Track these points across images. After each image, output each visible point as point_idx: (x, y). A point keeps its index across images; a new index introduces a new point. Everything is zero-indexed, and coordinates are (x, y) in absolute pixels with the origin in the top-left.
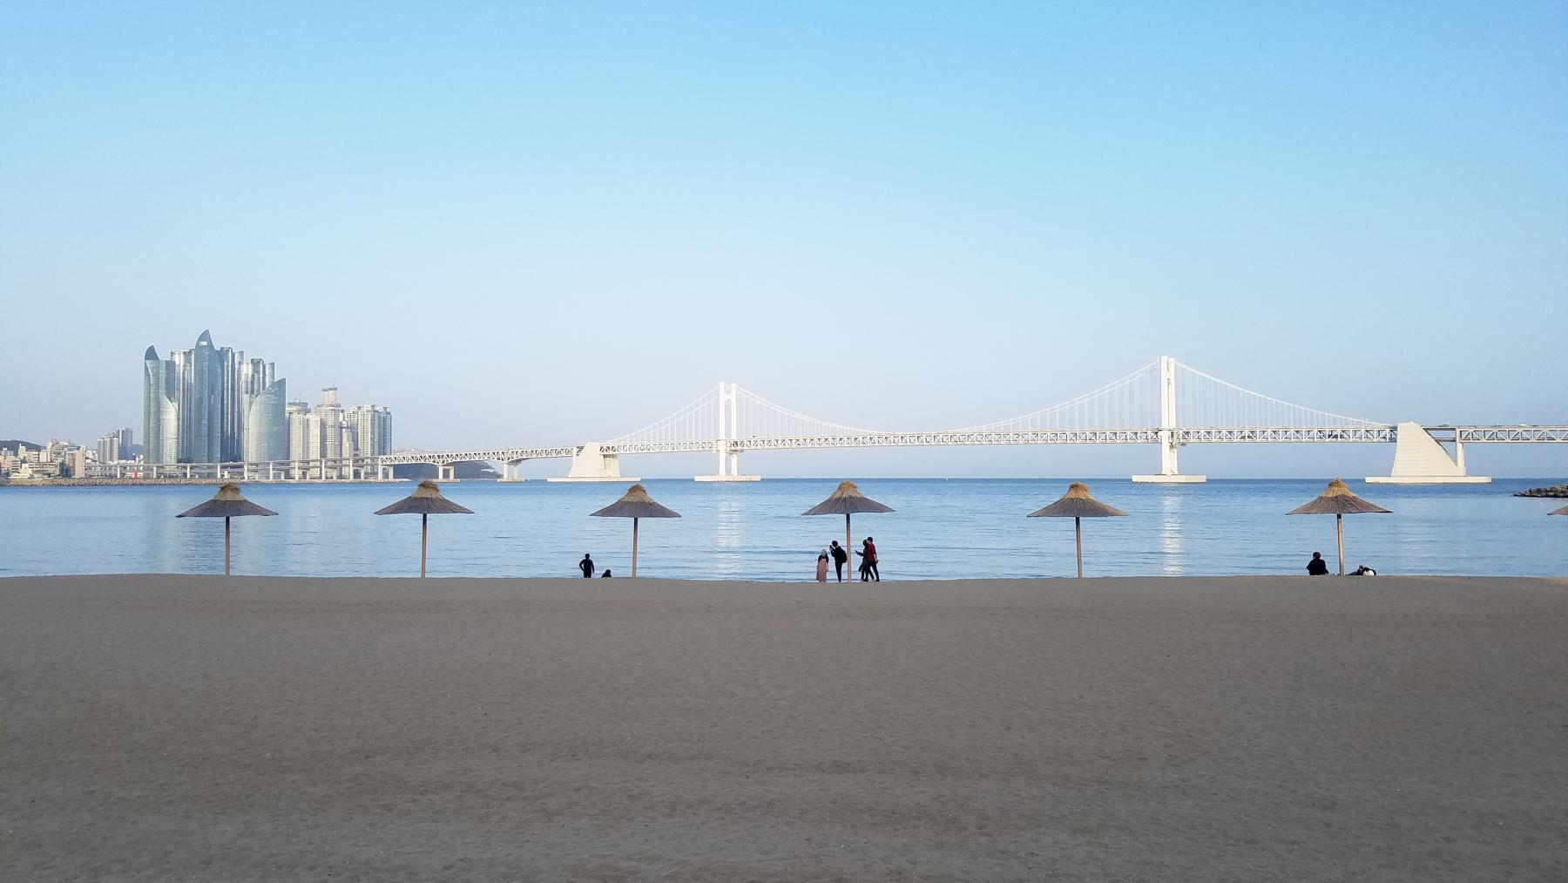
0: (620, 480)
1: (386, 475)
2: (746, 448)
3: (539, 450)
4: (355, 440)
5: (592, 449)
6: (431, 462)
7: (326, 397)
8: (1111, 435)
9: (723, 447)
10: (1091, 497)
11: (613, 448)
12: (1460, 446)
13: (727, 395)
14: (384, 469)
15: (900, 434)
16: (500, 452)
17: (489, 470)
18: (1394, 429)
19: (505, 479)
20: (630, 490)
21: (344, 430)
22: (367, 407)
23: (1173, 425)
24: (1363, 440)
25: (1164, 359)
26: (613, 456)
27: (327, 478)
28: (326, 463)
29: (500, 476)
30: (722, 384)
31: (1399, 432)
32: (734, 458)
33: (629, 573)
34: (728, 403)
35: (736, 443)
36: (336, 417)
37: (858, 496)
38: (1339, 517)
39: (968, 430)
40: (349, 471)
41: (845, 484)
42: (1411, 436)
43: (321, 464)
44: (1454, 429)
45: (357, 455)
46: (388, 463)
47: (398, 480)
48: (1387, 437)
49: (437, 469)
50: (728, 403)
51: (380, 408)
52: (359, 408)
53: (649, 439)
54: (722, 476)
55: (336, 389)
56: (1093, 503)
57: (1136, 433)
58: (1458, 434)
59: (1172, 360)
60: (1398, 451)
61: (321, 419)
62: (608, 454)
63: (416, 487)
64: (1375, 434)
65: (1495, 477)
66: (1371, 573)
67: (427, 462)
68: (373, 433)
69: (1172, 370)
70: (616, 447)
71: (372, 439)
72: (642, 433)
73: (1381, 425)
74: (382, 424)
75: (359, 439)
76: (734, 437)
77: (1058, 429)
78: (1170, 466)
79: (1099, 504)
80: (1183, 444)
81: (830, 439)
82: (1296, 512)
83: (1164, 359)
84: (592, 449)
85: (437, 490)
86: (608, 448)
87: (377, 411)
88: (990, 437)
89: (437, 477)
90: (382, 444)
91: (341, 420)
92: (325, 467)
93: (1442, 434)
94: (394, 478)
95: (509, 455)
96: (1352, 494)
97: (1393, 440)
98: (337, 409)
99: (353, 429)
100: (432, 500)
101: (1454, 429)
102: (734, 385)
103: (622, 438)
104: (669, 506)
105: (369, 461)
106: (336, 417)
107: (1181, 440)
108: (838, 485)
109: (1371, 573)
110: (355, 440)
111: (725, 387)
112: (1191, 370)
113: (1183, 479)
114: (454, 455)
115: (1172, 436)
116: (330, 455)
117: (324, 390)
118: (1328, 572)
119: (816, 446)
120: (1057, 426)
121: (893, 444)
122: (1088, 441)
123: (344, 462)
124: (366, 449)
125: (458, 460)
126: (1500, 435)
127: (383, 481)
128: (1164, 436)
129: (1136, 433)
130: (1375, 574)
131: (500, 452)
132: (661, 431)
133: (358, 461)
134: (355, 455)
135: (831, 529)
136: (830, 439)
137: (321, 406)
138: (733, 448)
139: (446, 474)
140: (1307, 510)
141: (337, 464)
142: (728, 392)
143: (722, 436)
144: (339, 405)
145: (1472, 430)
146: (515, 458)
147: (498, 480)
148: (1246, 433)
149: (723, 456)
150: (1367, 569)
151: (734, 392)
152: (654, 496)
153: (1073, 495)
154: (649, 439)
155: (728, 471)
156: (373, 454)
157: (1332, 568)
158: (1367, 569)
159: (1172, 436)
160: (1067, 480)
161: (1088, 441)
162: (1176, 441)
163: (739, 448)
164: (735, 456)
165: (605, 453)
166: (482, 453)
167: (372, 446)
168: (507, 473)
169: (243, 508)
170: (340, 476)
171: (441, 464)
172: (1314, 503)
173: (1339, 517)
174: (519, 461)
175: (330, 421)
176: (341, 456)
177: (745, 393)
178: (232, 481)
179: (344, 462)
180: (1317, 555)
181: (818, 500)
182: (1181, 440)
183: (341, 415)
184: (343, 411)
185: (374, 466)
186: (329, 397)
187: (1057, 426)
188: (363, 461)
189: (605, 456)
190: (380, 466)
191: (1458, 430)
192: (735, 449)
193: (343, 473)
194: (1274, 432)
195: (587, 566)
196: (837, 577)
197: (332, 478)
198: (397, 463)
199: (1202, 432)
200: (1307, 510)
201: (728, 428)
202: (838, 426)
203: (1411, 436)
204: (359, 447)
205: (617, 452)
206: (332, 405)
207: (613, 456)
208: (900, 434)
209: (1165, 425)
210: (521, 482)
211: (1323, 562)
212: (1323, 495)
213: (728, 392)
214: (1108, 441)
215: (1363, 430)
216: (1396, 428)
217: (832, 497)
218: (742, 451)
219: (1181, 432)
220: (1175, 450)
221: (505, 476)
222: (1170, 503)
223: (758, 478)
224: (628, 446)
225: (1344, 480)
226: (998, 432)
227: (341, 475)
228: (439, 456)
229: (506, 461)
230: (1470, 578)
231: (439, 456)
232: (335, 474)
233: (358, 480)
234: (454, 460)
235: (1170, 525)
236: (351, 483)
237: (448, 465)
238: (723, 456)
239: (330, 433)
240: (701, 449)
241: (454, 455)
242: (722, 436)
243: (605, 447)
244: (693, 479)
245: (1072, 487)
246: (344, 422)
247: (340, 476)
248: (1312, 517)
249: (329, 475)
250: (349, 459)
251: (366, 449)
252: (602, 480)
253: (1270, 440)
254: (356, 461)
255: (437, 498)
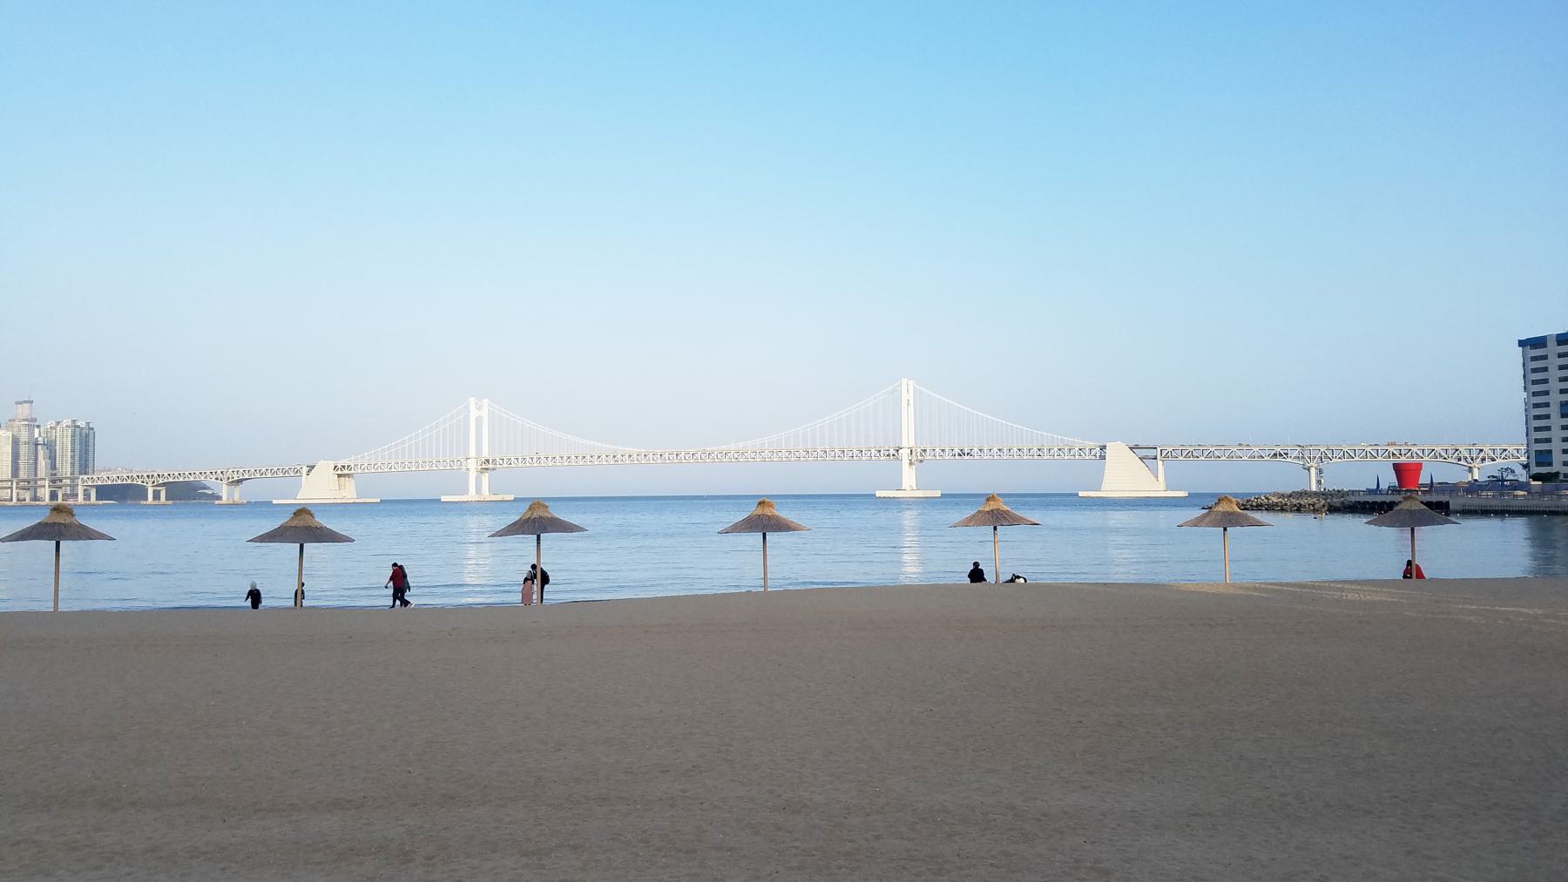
0: (357, 501)
1: (87, 496)
2: (498, 466)
3: (264, 470)
4: (52, 458)
5: (325, 468)
6: (139, 483)
7: (20, 410)
8: (822, 453)
9: (473, 465)
10: (777, 513)
11: (348, 466)
12: (1160, 463)
13: (479, 411)
14: (85, 490)
15: (659, 451)
16: (219, 472)
17: (206, 491)
18: (1103, 448)
19: (225, 500)
20: (295, 514)
21: (39, 447)
22: (67, 422)
23: (912, 444)
24: (1077, 457)
25: (904, 381)
26: (348, 475)
27: (18, 500)
28: (17, 483)
29: (220, 498)
30: (472, 400)
31: (1108, 450)
32: (485, 477)
33: (49, 607)
34: (479, 420)
35: (488, 461)
36: (31, 433)
37: (549, 516)
38: (995, 529)
39: (724, 448)
40: (45, 493)
41: (537, 504)
42: (1118, 452)
43: (12, 484)
44: (1156, 448)
45: (55, 475)
46: (90, 484)
47: (101, 502)
48: (1098, 455)
49: (145, 490)
50: (479, 420)
51: (82, 424)
52: (58, 423)
53: (383, 458)
54: (472, 495)
55: (31, 402)
56: (777, 518)
57: (880, 451)
58: (1159, 451)
59: (912, 382)
60: (1107, 467)
61: (13, 435)
62: (343, 473)
63: (49, 511)
64: (1087, 452)
65: (383, 499)
66: (1022, 580)
67: (135, 482)
68: (73, 451)
69: (911, 391)
70: (353, 466)
71: (73, 457)
72: (383, 450)
73: (1092, 444)
74: (84, 441)
75: (57, 456)
76: (485, 454)
77: (827, 448)
78: (909, 483)
79: (784, 519)
80: (921, 461)
81: (588, 457)
82: (1186, 524)
83: (904, 381)
84: (325, 468)
85: (73, 515)
86: (344, 467)
87: (78, 427)
88: (729, 455)
89: (147, 499)
90: (84, 462)
91: (36, 436)
92: (17, 488)
93: (1146, 453)
94: (97, 499)
95: (229, 474)
96: (1006, 508)
97: (1103, 458)
98: (32, 423)
99: (50, 447)
100: (65, 525)
101: (1156, 448)
102: (486, 401)
103: (359, 456)
104: (342, 530)
105: (68, 482)
106: (31, 433)
107: (919, 458)
108: (529, 504)
109: (1022, 580)
110: (52, 458)
111: (476, 404)
112: (928, 392)
113: (920, 494)
114: (166, 474)
115: (911, 454)
116: (23, 474)
117: (18, 403)
118: (985, 580)
119: (574, 464)
120: (783, 445)
121: (652, 462)
122: (837, 459)
123: (39, 483)
124: (65, 468)
125: (171, 480)
126: (1195, 454)
127: (84, 502)
128: (904, 453)
129: (880, 451)
130: (1026, 581)
131: (219, 472)
132: (404, 448)
133: (55, 481)
134: (52, 475)
135: (522, 552)
136: (588, 457)
137: (14, 420)
138: (484, 467)
139: (156, 496)
140: (967, 523)
141: (31, 485)
142: (479, 408)
143: (472, 453)
144: (35, 420)
145: (1214, 449)
146: (236, 478)
147: (217, 502)
148: (957, 451)
149: (473, 475)
150: (1019, 577)
151: (485, 408)
152: (784, 513)
153: (760, 511)
154: (383, 458)
155: (478, 490)
156: (72, 474)
157: (989, 576)
158: (1019, 577)
159: (911, 454)
160: (985, 494)
161: (837, 459)
162: (914, 458)
163: (491, 466)
164: (486, 474)
165: (339, 472)
166: (208, 472)
167: (73, 464)
168: (225, 493)
169: (781, 526)
170: (35, 498)
171: (150, 484)
172: (974, 516)
173: (995, 529)
174: (239, 481)
175: (24, 437)
176: (36, 475)
177: (505, 413)
178: (64, 502)
179: (39, 483)
180: (976, 564)
181: (741, 516)
182: (919, 458)
183: (36, 430)
184: (38, 426)
185: (74, 487)
186: (24, 411)
187: (783, 445)
188: (61, 481)
189: (339, 476)
190: (80, 487)
191: (1159, 449)
192: (486, 466)
193: (38, 495)
194: (1000, 450)
195: (255, 596)
196: (293, 603)
197: (24, 500)
198: (100, 483)
199: (937, 450)
200: (967, 523)
201: (480, 444)
202: (596, 444)
203: (1118, 452)
204: (57, 466)
205: (353, 471)
206: (24, 420)
207: (348, 475)
208: (659, 452)
209: (904, 444)
210: (242, 505)
211: (982, 570)
212: (980, 509)
213: (479, 408)
214: (873, 458)
215: (1077, 449)
216: (1105, 447)
217: (520, 519)
218: (494, 469)
219: (919, 450)
220: (914, 467)
221: (224, 498)
222: (909, 518)
223: (512, 497)
224: (366, 464)
225: (999, 495)
226: (754, 449)
227: (35, 497)
228: (148, 476)
229: (225, 481)
230: (1105, 584)
231: (138, 476)
232: (27, 495)
233: (156, 502)
234: (166, 481)
235: (909, 539)
236: (47, 505)
237: (158, 485)
238: (473, 475)
239: (23, 450)
240: (448, 468)
241: (166, 474)
242: (472, 453)
243: (339, 466)
244: (440, 500)
245: (760, 504)
246: (40, 439)
247: (35, 498)
248: (971, 530)
249: (22, 497)
250: (45, 479)
251: (65, 468)
252: (335, 501)
253: (1015, 457)
254: (54, 481)
255: (72, 523)
